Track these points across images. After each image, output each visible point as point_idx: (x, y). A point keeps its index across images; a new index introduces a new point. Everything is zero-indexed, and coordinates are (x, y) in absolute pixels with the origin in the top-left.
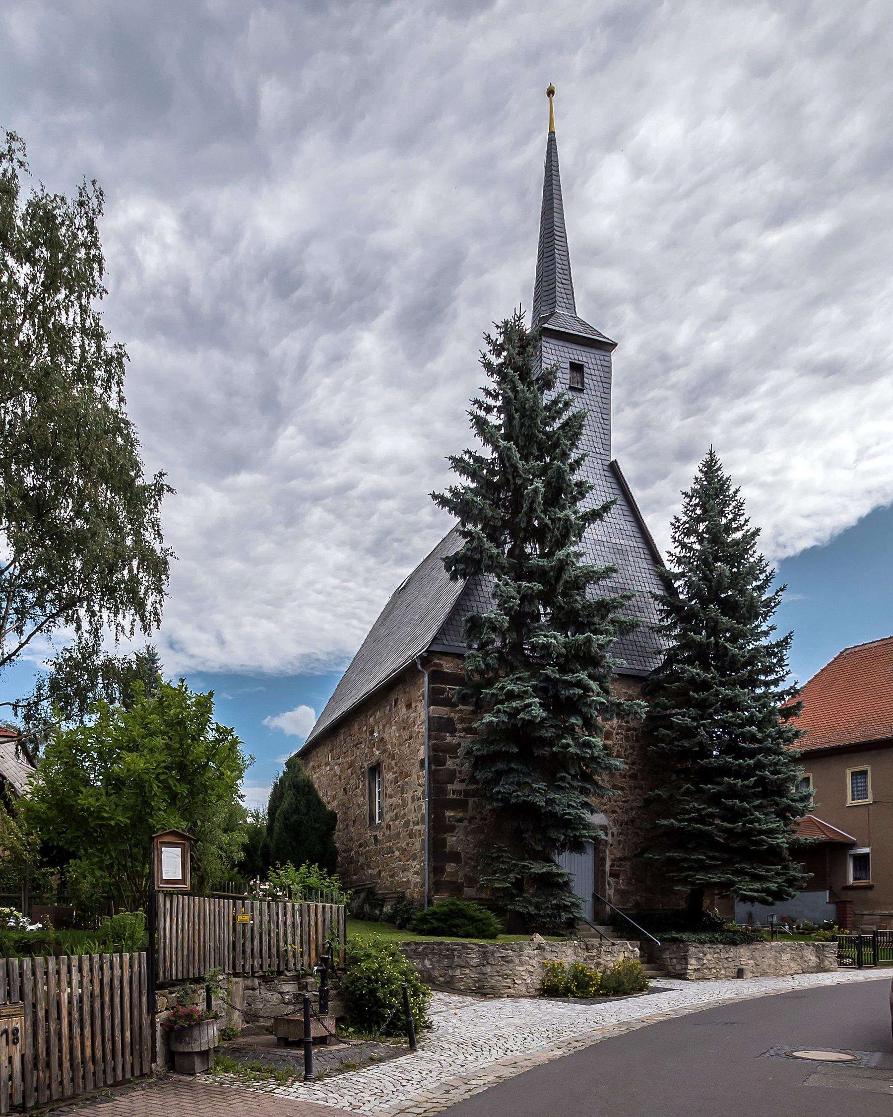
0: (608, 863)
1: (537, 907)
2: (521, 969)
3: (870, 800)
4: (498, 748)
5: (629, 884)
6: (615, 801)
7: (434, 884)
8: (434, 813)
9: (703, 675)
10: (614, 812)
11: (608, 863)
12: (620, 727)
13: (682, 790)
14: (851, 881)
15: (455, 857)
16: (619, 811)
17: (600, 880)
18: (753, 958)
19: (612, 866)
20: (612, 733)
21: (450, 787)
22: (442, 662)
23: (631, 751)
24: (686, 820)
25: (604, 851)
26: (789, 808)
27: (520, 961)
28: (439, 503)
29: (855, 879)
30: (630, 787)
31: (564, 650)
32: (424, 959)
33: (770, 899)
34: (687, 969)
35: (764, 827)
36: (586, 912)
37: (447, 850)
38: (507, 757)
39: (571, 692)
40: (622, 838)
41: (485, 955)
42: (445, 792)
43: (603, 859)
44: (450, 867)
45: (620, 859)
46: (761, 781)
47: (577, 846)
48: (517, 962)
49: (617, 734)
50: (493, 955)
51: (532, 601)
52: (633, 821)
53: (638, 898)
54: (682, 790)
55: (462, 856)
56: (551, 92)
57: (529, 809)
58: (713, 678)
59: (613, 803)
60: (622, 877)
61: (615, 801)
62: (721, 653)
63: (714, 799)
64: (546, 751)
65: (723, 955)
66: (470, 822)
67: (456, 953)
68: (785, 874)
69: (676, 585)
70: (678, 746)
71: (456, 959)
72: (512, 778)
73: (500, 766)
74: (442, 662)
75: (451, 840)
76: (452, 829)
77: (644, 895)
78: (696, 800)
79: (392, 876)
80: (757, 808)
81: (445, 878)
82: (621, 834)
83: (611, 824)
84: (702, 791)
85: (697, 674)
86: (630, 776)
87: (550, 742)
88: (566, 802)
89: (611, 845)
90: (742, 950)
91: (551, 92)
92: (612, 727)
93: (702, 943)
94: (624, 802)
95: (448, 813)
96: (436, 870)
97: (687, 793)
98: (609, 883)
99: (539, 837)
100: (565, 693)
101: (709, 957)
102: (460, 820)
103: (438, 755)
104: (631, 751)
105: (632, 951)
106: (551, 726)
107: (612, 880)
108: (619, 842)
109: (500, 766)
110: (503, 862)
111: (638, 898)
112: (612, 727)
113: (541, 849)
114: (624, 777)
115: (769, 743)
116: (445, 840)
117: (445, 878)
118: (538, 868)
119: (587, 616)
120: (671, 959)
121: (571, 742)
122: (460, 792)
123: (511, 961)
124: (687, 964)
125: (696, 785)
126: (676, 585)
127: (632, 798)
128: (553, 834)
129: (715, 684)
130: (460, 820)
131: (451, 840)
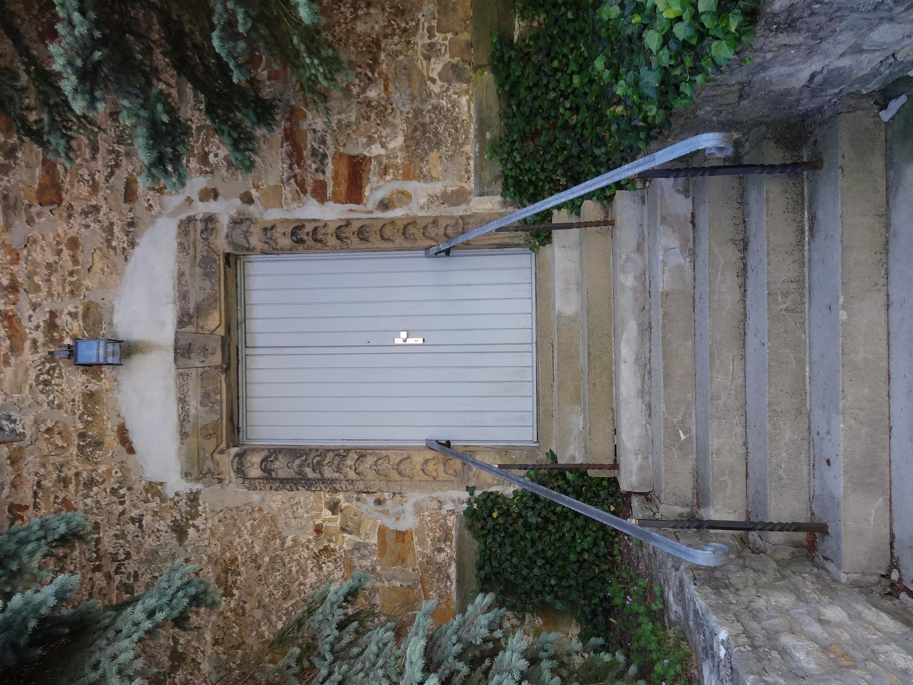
6: (95, 188)
10: (130, 195)
11: (312, 210)
45: (296, 156)
53: (436, 67)
60: (357, 148)
77: (421, 40)
83: (174, 200)
89: (247, 199)
98: (384, 205)
107: (377, 189)
111: (436, 67)
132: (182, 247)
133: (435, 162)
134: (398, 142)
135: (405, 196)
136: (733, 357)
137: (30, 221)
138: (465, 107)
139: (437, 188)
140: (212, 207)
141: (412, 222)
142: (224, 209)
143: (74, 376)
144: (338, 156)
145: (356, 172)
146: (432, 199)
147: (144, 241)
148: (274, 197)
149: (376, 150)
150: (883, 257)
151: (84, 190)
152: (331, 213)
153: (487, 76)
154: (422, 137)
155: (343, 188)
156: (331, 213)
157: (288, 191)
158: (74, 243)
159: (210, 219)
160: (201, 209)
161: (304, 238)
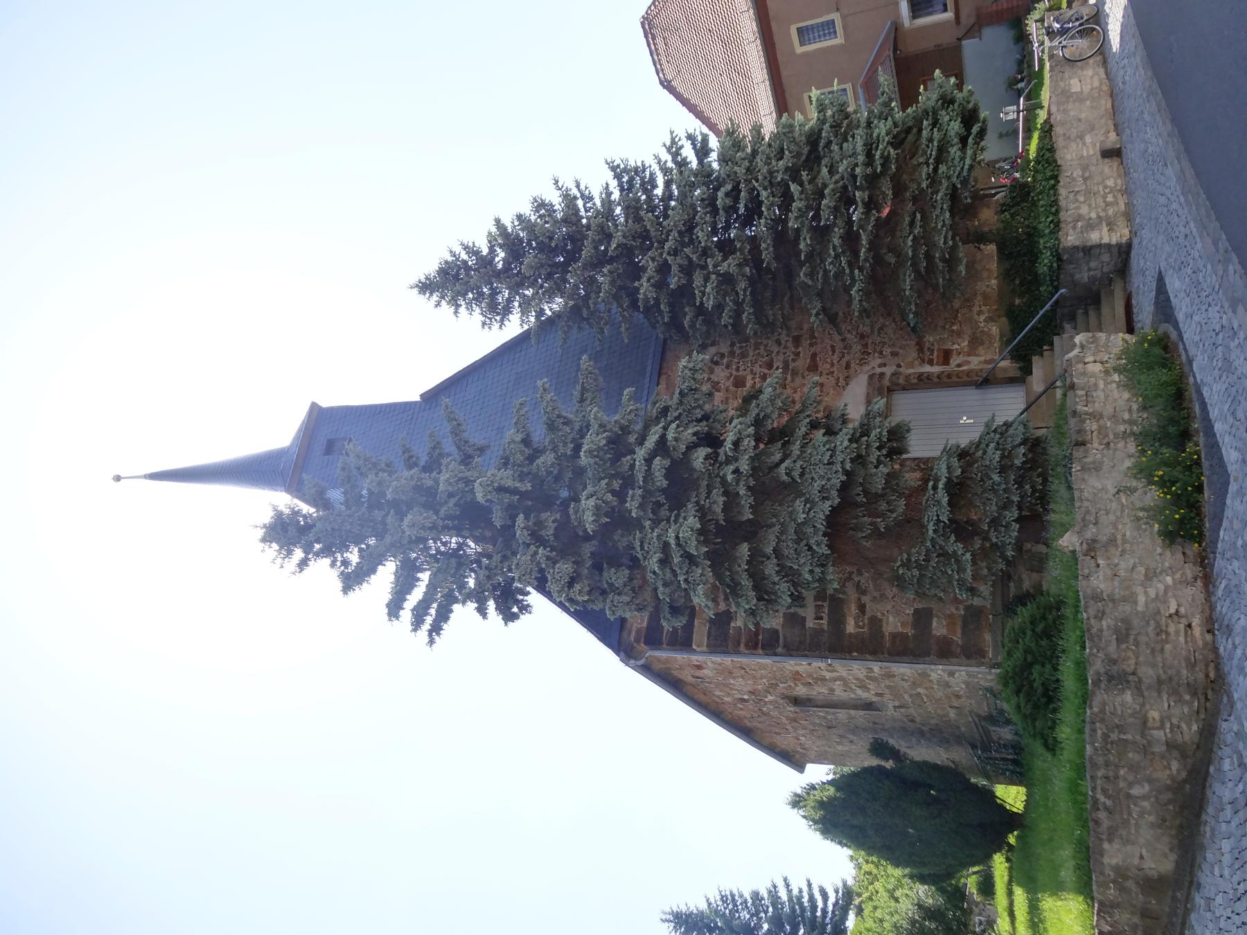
0: (927, 369)
1: (1006, 506)
2: (1142, 599)
3: (835, 16)
4: (745, 576)
5: (959, 334)
6: (833, 365)
7: (968, 657)
8: (850, 652)
9: (650, 271)
10: (848, 366)
11: (927, 369)
12: (728, 367)
13: (810, 283)
14: (949, 15)
15: (922, 618)
16: (847, 358)
17: (955, 379)
18: (1081, 137)
19: (931, 363)
20: (736, 377)
21: (810, 623)
22: (634, 629)
23: (762, 347)
24: (852, 272)
25: (908, 377)
26: (836, 126)
27: (1125, 599)
28: (439, 634)
29: (945, 10)
30: (811, 345)
31: (604, 482)
32: (1128, 796)
33: (975, 129)
34: (1109, 246)
35: (861, 158)
36: (1008, 405)
37: (909, 631)
38: (756, 557)
39: (657, 474)
40: (887, 351)
41: (1118, 679)
42: (818, 632)
43: (920, 376)
44: (939, 628)
45: (921, 349)
46: (794, 173)
47: (895, 441)
48: (1127, 608)
49: (738, 369)
50: (1114, 662)
51: (541, 522)
52: (862, 336)
53: (982, 318)
54: (810, 283)
55: (920, 606)
56: (118, 478)
57: (835, 523)
58: (653, 259)
59: (835, 369)
60: (948, 346)
61: (833, 365)
62: (626, 252)
63: (822, 233)
64: (746, 500)
65: (1080, 186)
66: (864, 592)
67: (1114, 736)
68: (935, 112)
69: (549, 313)
70: (745, 295)
71: (1129, 737)
72: (788, 550)
73: (770, 569)
74: (634, 629)
75: (893, 624)
76: (876, 623)
77: (976, 309)
78: (823, 261)
79: (958, 697)
80: (832, 171)
81: (957, 638)
82: (881, 353)
83: (866, 368)
84: (810, 255)
85: (648, 281)
86: (797, 347)
87: (731, 498)
88: (820, 467)
89: (899, 366)
90: (1068, 157)
91: (118, 478)
92: (728, 378)
93: (1057, 225)
94: (834, 352)
95: (851, 627)
96: (945, 652)
97: (811, 275)
98: (959, 366)
99: (883, 506)
100: (660, 481)
101: (1084, 210)
102: (862, 608)
103: (764, 643)
104: (762, 347)
105: (1082, 347)
106: (709, 493)
107: (954, 361)
108: (894, 354)
109: (770, 569)
110: (927, 560)
111: (982, 318)
112: (728, 378)
113: (903, 502)
114: (798, 354)
115: (740, 171)
116: (894, 636)
117: (957, 638)
118: (938, 508)
119: (565, 444)
120: (1090, 269)
121: (732, 468)
122: (818, 607)
123: (1127, 621)
124: (1100, 246)
125: (802, 264)
126: (549, 313)
127: (827, 341)
128: (878, 484)
129: (661, 254)
130: (862, 608)
131: (893, 624)
132: (869, 384)
133: (981, 350)
134: (966, 343)
135: (968, 363)
136: (869, 706)
137: (804, 377)
138: (995, 330)
139: (982, 358)
140: (883, 370)
141: (972, 371)
142: (888, 371)
143: (455, 505)
144: (939, 350)
145: (946, 357)
146: (980, 362)
147: (853, 384)
148: (911, 365)
149: (956, 346)
150: (1085, 863)
151: (828, 366)
152: (936, 369)
153: (1004, 319)
154: (976, 342)
155: (941, 360)
156: (936, 369)
157: (916, 363)
158: (822, 385)
159: (882, 374)
160: (878, 370)
161: (924, 382)
